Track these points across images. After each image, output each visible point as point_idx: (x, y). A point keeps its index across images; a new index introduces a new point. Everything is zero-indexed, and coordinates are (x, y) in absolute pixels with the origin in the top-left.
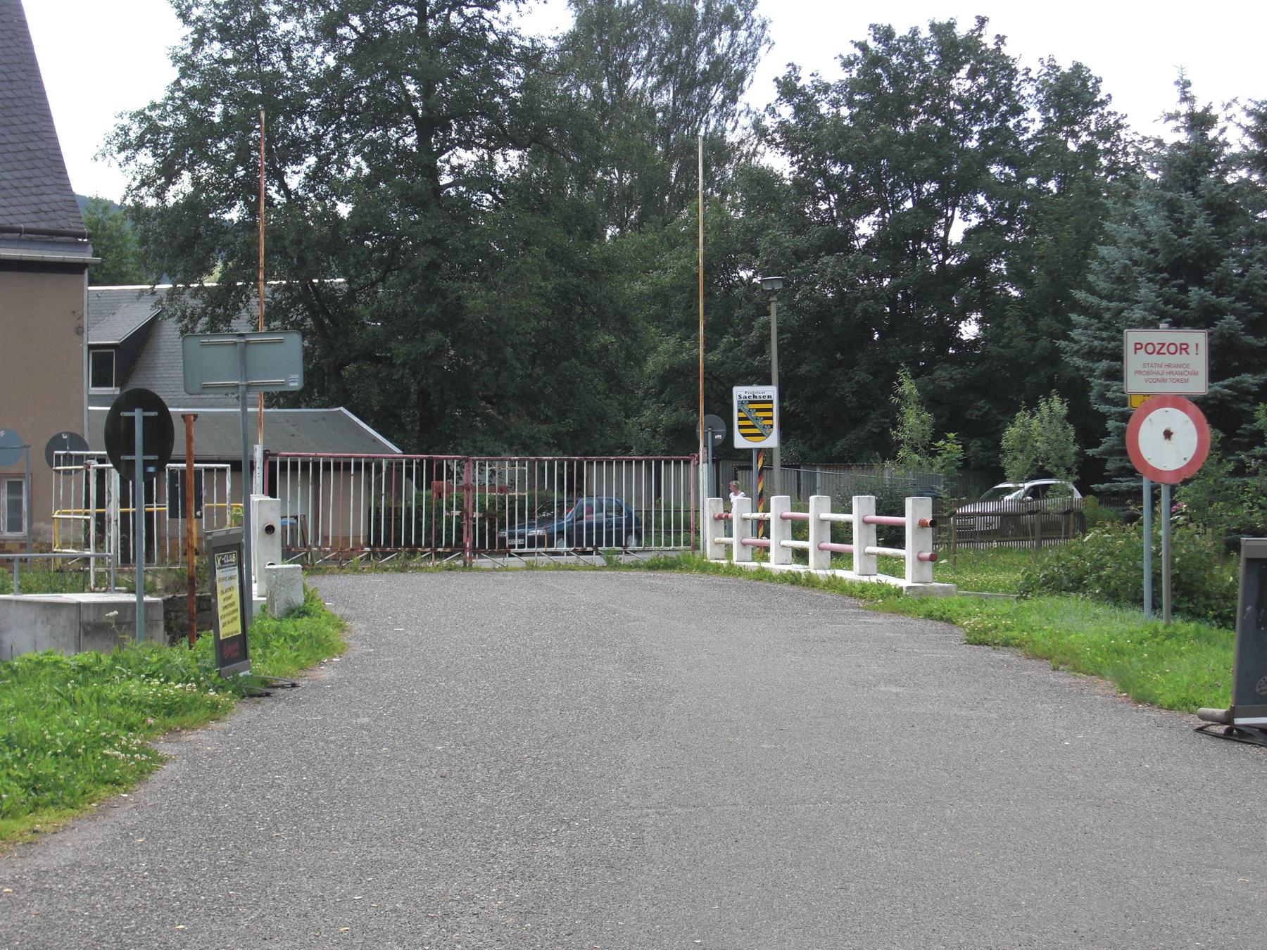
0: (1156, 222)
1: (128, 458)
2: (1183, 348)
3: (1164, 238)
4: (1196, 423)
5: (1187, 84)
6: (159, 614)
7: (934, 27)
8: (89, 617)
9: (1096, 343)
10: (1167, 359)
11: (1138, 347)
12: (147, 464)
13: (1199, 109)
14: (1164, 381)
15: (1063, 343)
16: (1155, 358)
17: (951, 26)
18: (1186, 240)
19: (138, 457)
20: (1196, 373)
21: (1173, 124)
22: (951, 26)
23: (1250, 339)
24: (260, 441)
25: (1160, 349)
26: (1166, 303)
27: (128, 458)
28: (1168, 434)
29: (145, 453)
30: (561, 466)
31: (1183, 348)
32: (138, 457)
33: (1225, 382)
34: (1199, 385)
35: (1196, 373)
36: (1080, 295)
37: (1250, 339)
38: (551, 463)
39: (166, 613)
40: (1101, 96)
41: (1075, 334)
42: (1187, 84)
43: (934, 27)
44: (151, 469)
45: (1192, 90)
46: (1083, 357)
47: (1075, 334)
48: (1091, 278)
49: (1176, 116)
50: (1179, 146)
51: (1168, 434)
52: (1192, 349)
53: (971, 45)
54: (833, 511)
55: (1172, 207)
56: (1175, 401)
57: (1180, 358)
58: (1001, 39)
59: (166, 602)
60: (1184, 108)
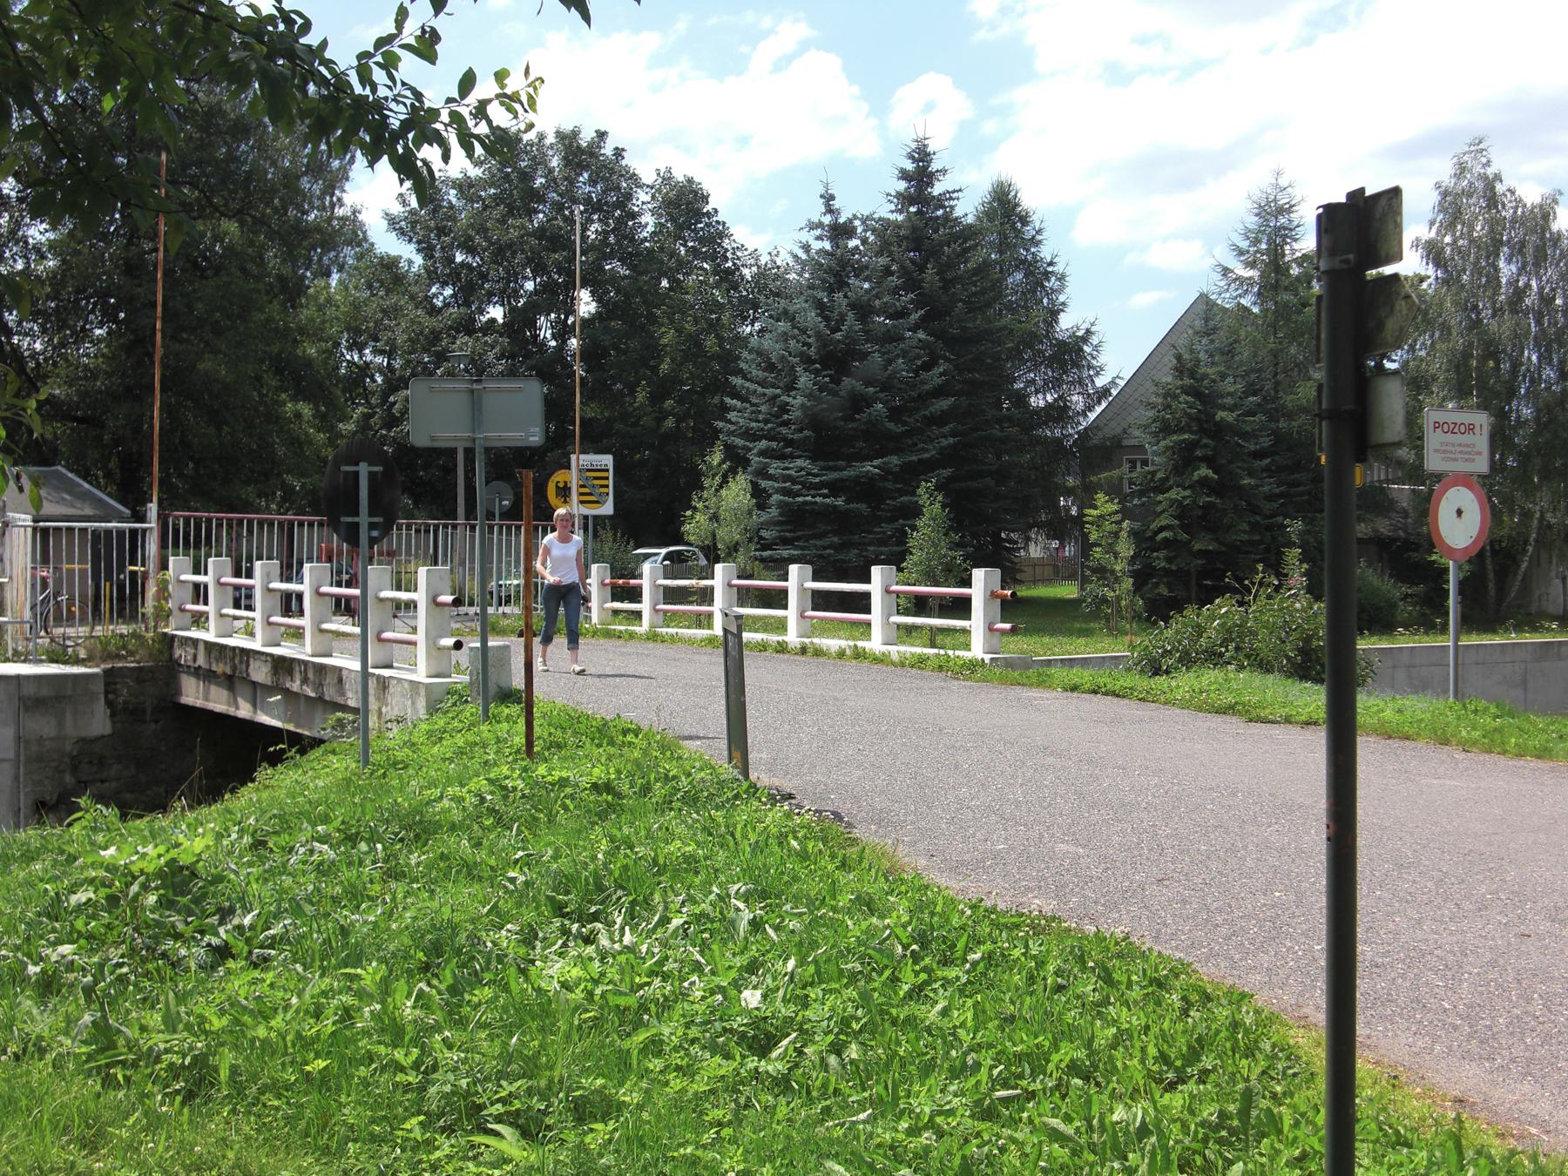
0: (812, 317)
1: (349, 519)
2: (1470, 428)
3: (818, 335)
4: (1439, 500)
5: (832, 198)
6: (99, 687)
7: (560, 135)
8: (29, 690)
9: (754, 424)
10: (1458, 438)
11: (1437, 425)
12: (372, 526)
13: (841, 221)
14: (1456, 460)
15: (720, 424)
16: (1450, 438)
17: (575, 134)
18: (838, 336)
19: (364, 519)
20: (1480, 453)
21: (818, 232)
22: (575, 134)
23: (891, 426)
24: (155, 499)
25: (1453, 428)
26: (821, 390)
27: (349, 519)
28: (1459, 513)
29: (371, 514)
30: (220, 525)
31: (1470, 428)
32: (364, 519)
33: (875, 463)
34: (1482, 465)
35: (1480, 453)
36: (737, 381)
37: (891, 426)
38: (209, 520)
39: (107, 684)
40: (708, 208)
41: (732, 416)
42: (832, 198)
43: (560, 135)
44: (375, 534)
45: (836, 204)
46: (741, 436)
47: (732, 416)
48: (743, 365)
49: (820, 225)
50: (822, 252)
51: (1459, 513)
52: (1477, 430)
53: (593, 150)
54: (814, 579)
55: (820, 306)
56: (1464, 480)
57: (1466, 439)
58: (619, 152)
59: (106, 672)
60: (827, 220)
